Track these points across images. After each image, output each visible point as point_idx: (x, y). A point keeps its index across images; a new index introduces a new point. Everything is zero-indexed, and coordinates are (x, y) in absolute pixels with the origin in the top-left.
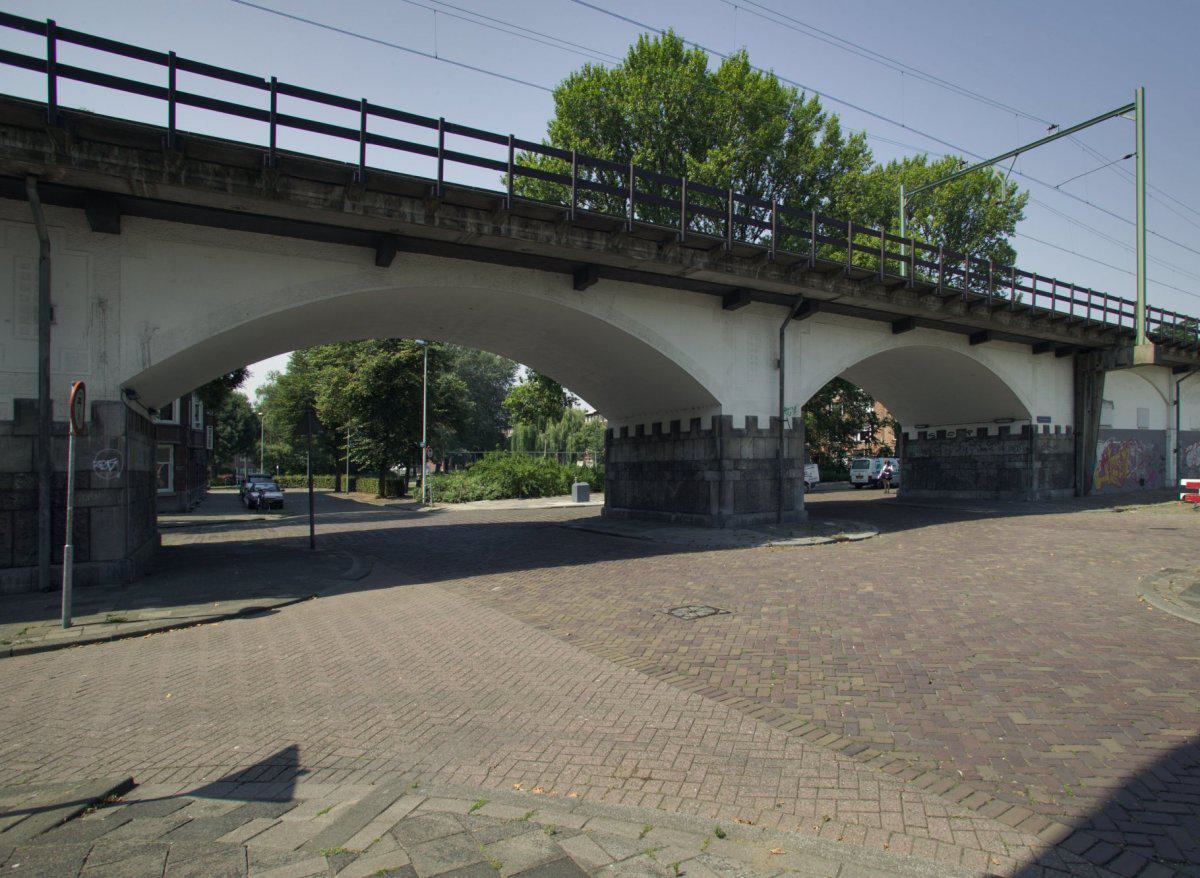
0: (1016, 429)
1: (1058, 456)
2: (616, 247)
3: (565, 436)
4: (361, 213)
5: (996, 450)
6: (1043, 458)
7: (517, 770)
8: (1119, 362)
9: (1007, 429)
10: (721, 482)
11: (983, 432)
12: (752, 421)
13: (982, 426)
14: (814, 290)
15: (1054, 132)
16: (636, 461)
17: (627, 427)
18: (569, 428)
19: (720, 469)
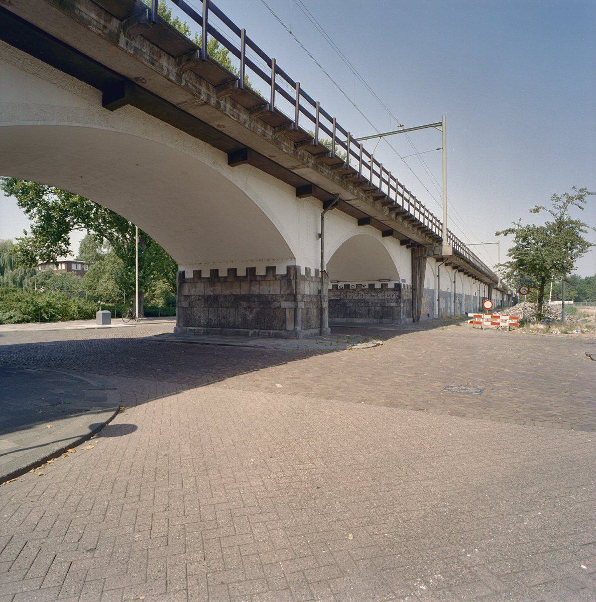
0: (391, 285)
1: (408, 300)
2: (276, 139)
3: (22, 278)
4: (132, 52)
5: (380, 296)
6: (404, 301)
7: (60, 521)
8: (435, 253)
9: (386, 285)
10: (295, 310)
11: (372, 286)
12: (308, 270)
13: (372, 283)
14: (346, 195)
15: (401, 129)
16: (211, 294)
17: (201, 271)
18: (25, 273)
19: (295, 300)
